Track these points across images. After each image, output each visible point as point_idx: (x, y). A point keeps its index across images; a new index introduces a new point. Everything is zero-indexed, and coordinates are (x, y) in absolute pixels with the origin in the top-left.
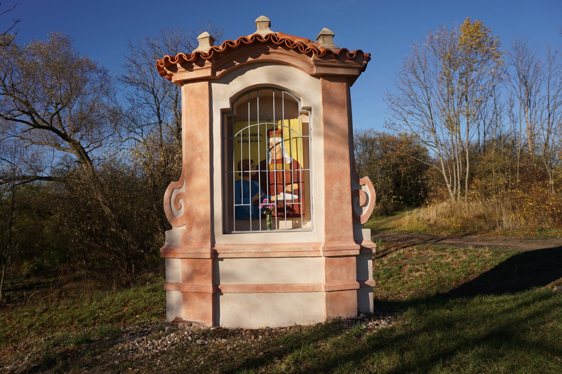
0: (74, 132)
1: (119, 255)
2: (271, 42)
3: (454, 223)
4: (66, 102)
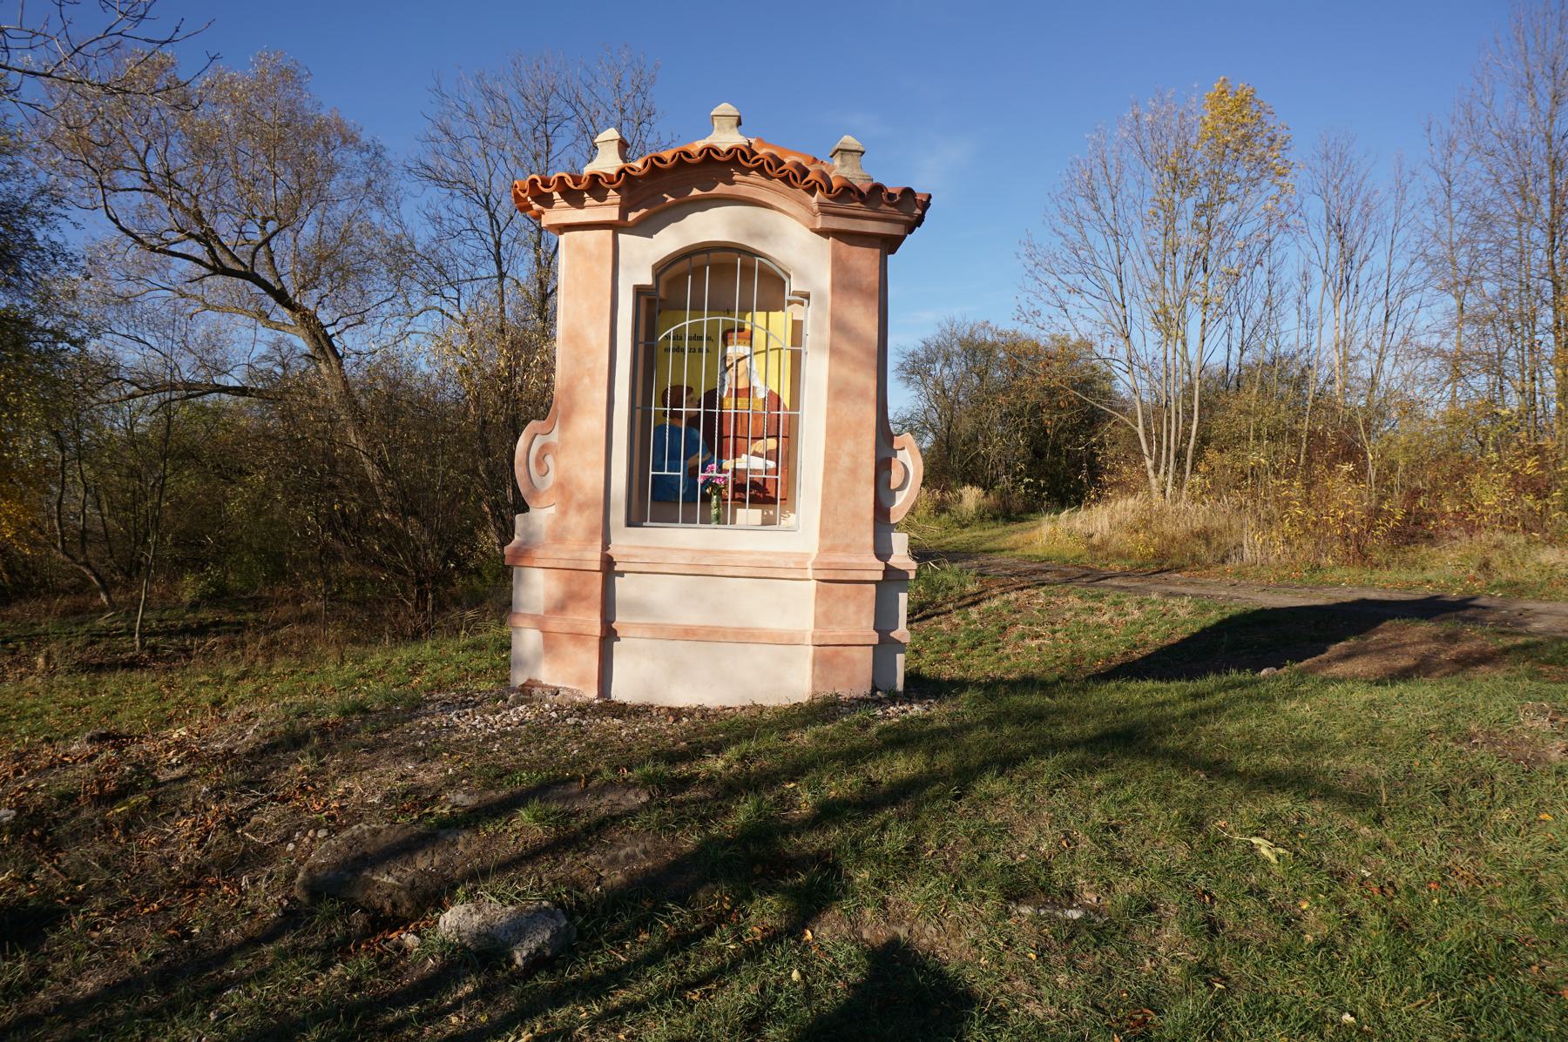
0: (304, 287)
1: (399, 570)
2: (739, 160)
3: (1140, 545)
4: (287, 218)
